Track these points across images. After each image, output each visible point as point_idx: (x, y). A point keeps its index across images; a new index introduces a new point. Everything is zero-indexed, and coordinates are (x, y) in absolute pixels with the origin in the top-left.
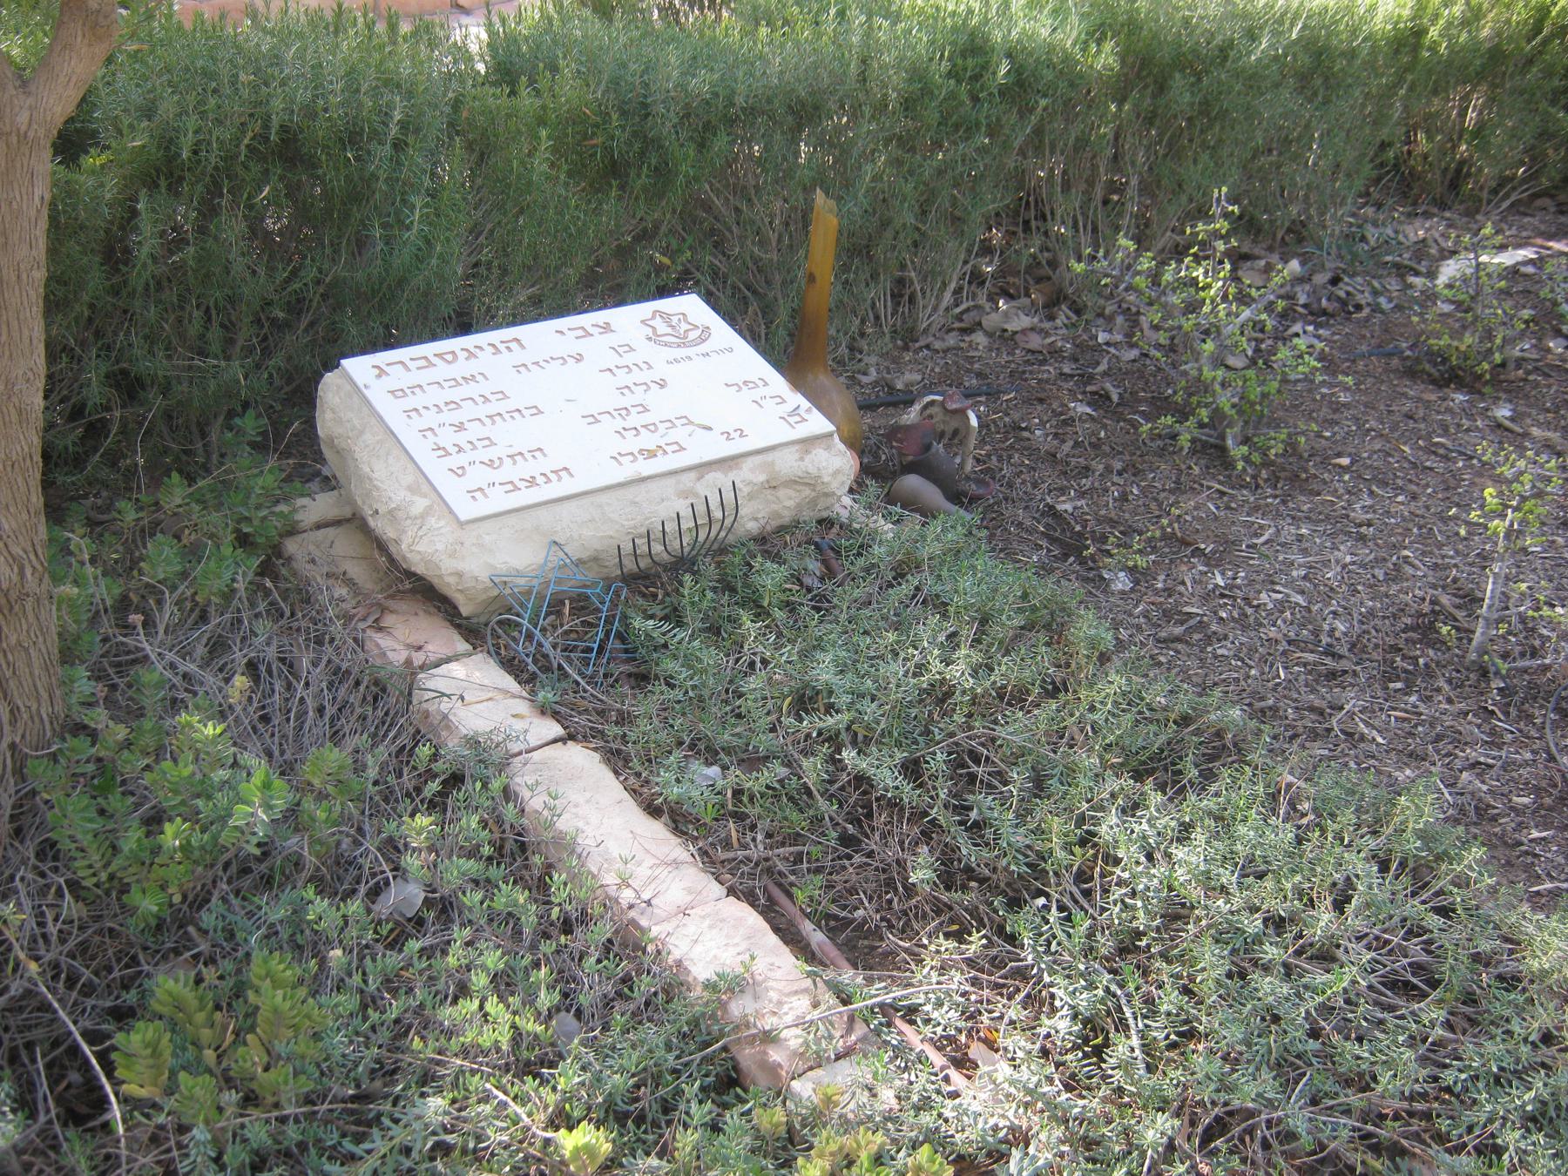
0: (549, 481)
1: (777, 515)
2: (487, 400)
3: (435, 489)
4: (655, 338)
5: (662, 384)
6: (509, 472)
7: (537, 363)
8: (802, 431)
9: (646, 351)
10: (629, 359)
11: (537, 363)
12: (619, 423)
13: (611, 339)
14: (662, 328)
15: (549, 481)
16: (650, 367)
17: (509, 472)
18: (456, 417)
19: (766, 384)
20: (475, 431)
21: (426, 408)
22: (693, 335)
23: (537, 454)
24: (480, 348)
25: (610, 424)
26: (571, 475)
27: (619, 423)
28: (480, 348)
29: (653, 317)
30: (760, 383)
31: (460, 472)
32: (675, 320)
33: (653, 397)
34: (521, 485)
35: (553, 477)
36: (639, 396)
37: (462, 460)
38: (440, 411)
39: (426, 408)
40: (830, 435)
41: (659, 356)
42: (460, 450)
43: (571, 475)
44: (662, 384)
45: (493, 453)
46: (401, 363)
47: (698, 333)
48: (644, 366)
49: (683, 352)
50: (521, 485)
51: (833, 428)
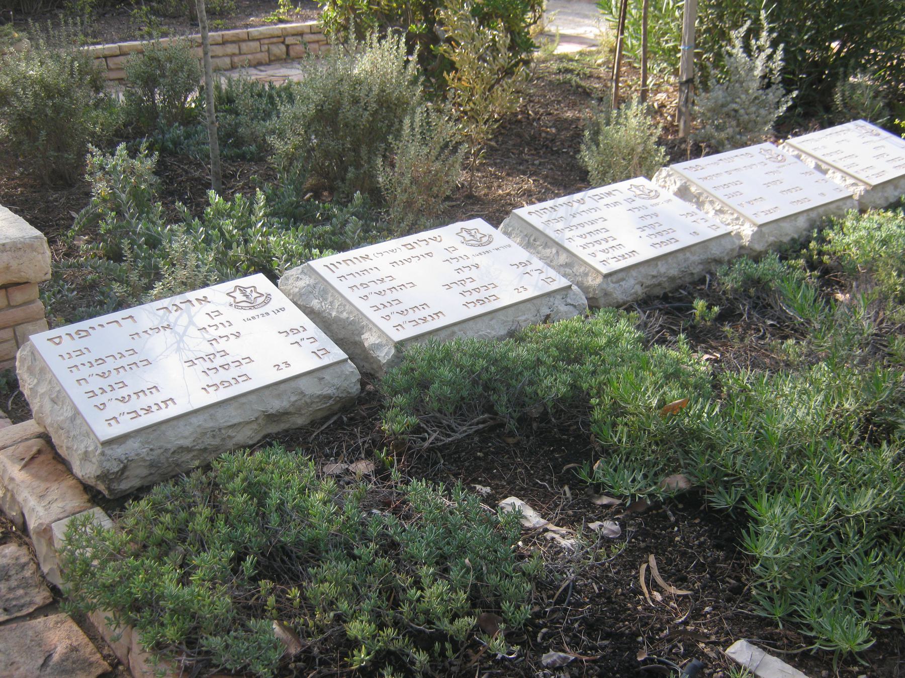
0: (433, 319)
1: (41, 524)
2: (123, 356)
3: (376, 326)
4: (237, 305)
5: (237, 335)
6: (412, 316)
7: (146, 332)
8: (326, 361)
9: (463, 250)
10: (217, 320)
11: (146, 332)
12: (461, 288)
13: (209, 308)
14: (239, 296)
15: (160, 408)
16: (231, 325)
17: (412, 316)
18: (104, 368)
19: (305, 330)
20: (114, 378)
21: (83, 364)
22: (485, 239)
23: (154, 390)
24: (93, 328)
25: (202, 365)
26: (175, 403)
27: (461, 288)
28: (93, 328)
29: (235, 291)
30: (301, 330)
31: (387, 318)
32: (248, 291)
33: (474, 273)
34: (142, 412)
35: (163, 405)
36: (466, 274)
37: (103, 398)
38: (92, 365)
39: (83, 364)
40: (345, 361)
41: (236, 316)
42: (104, 391)
43: (175, 403)
44: (237, 335)
45: (124, 392)
46: (117, 322)
47: (262, 299)
48: (227, 324)
49: (254, 312)
50: (142, 412)
51: (347, 356)
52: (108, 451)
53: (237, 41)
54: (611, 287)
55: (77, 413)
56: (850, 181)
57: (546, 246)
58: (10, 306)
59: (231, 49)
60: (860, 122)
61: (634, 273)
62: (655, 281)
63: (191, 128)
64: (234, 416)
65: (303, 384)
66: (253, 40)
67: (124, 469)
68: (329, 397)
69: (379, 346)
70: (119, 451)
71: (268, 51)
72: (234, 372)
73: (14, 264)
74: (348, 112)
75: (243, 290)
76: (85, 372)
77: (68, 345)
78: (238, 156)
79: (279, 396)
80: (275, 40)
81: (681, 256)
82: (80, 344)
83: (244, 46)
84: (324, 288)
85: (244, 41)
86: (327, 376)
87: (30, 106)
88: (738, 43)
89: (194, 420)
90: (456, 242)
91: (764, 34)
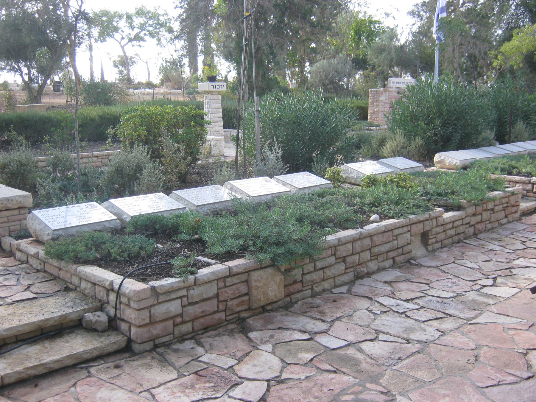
4: (88, 207)
52: (54, 232)
53: (88, 157)
54: (199, 209)
55: (46, 225)
56: (292, 187)
57: (181, 200)
58: (19, 214)
59: (85, 160)
60: (306, 172)
61: (207, 206)
62: (215, 210)
63: (70, 182)
64: (86, 229)
65: (105, 223)
66: (95, 157)
67: (58, 238)
68: (112, 228)
69: (126, 218)
70: (57, 233)
71: (101, 162)
72: (87, 219)
73: (22, 201)
74: (127, 170)
75: (89, 205)
76: (47, 218)
77: (42, 213)
78: (88, 191)
79: (98, 226)
80: (104, 157)
81: (223, 203)
82: (46, 213)
83: (91, 159)
84: (113, 206)
85: (90, 157)
86: (112, 222)
87: (15, 168)
88: (267, 148)
89: (77, 228)
90: (154, 199)
91: (276, 145)
